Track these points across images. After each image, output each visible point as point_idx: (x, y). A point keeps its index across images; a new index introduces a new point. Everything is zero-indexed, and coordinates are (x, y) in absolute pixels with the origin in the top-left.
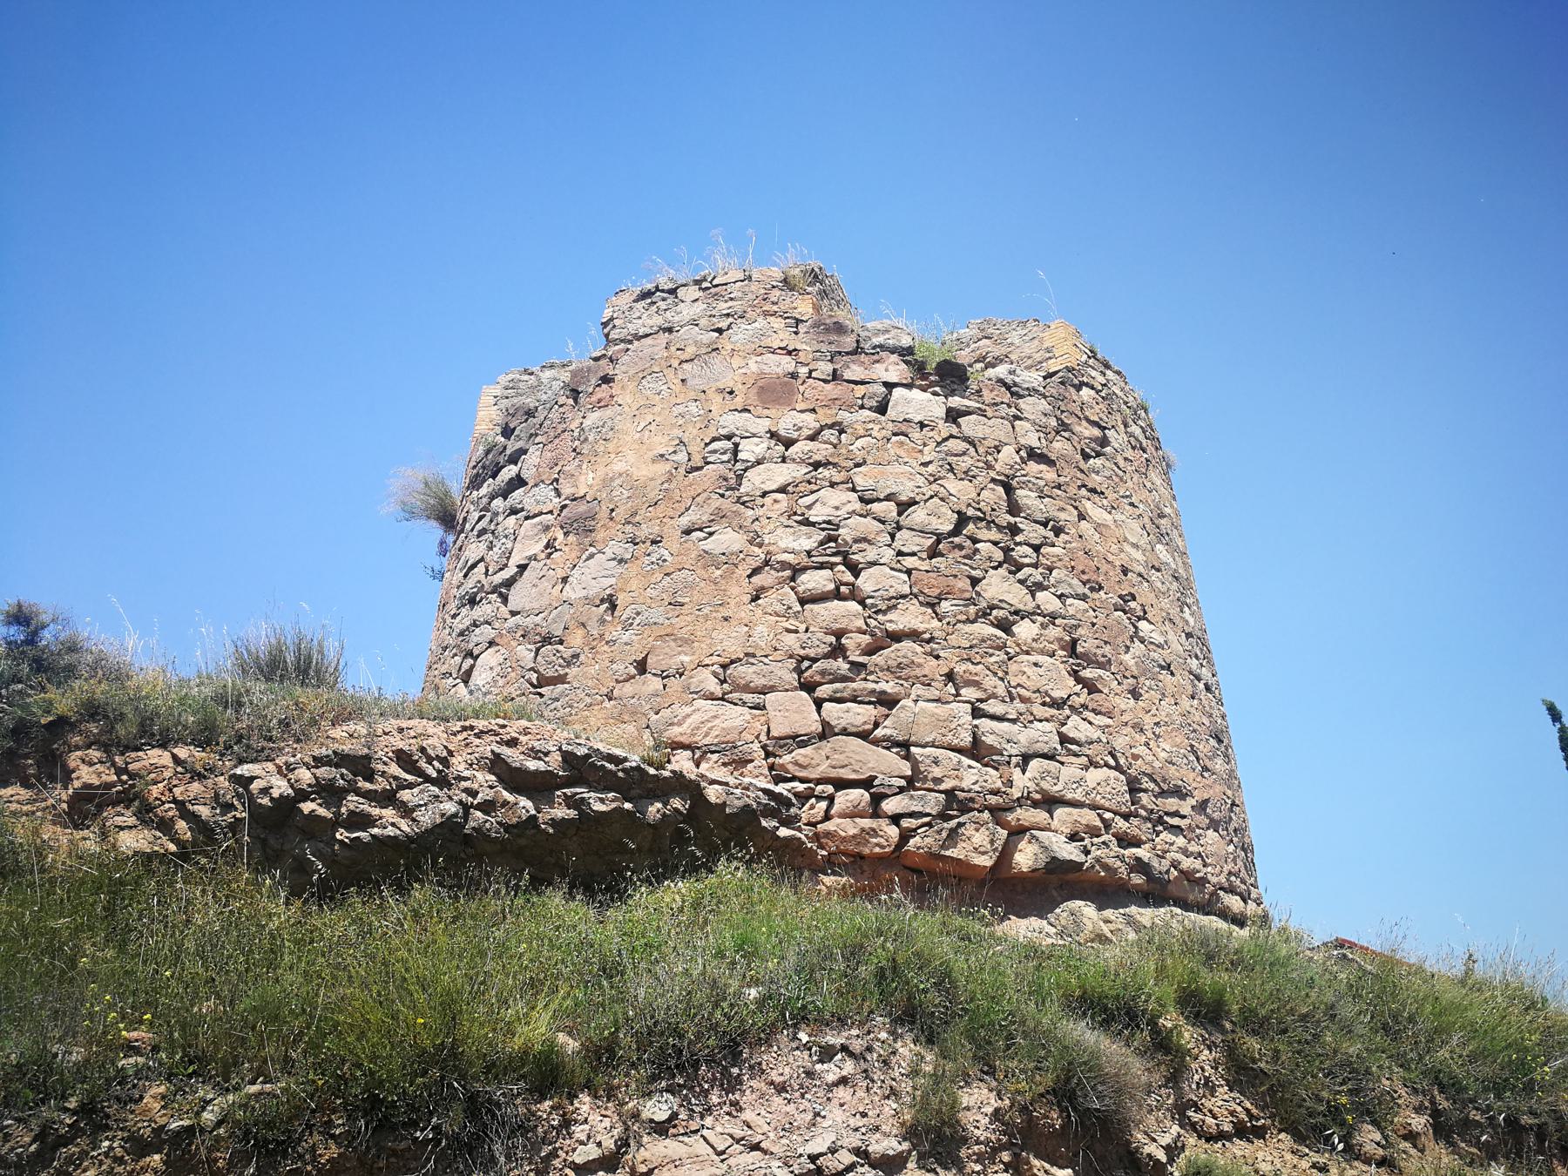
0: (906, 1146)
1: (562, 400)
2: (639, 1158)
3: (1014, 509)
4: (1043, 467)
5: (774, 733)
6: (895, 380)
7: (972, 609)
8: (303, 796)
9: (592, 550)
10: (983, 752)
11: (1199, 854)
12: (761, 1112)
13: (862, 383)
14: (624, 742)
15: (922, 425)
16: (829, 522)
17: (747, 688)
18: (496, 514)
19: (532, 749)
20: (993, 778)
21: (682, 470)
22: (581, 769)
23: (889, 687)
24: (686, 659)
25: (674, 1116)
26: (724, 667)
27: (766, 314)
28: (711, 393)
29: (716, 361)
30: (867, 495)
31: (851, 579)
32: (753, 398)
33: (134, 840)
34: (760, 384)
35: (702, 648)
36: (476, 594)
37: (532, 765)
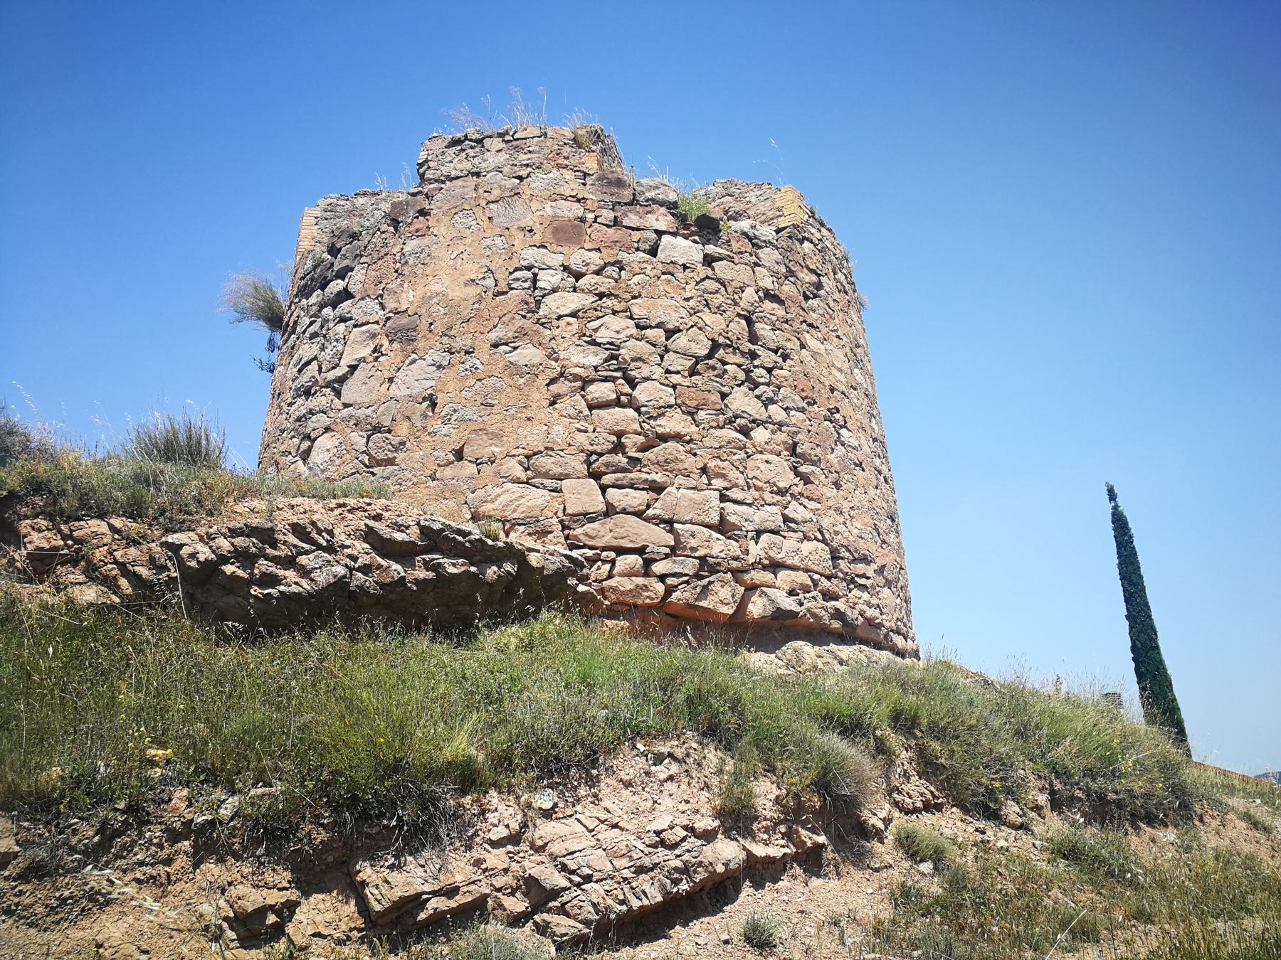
0: (717, 823)
1: (384, 227)
2: (537, 836)
3: (754, 338)
4: (775, 305)
5: (569, 511)
6: (664, 228)
7: (721, 418)
8: (224, 560)
9: (414, 356)
10: (727, 528)
12: (614, 800)
13: (638, 229)
14: (445, 514)
15: (685, 267)
16: (611, 344)
17: (547, 475)
18: (326, 321)
19: (396, 523)
20: (734, 548)
21: (490, 294)
22: (435, 540)
23: (658, 477)
24: (497, 450)
25: (555, 805)
26: (528, 457)
27: (559, 166)
28: (513, 230)
29: (518, 204)
30: (642, 322)
31: (629, 391)
32: (549, 237)
33: (89, 594)
34: (555, 224)
35: (510, 442)
36: (311, 387)
37: (399, 536)
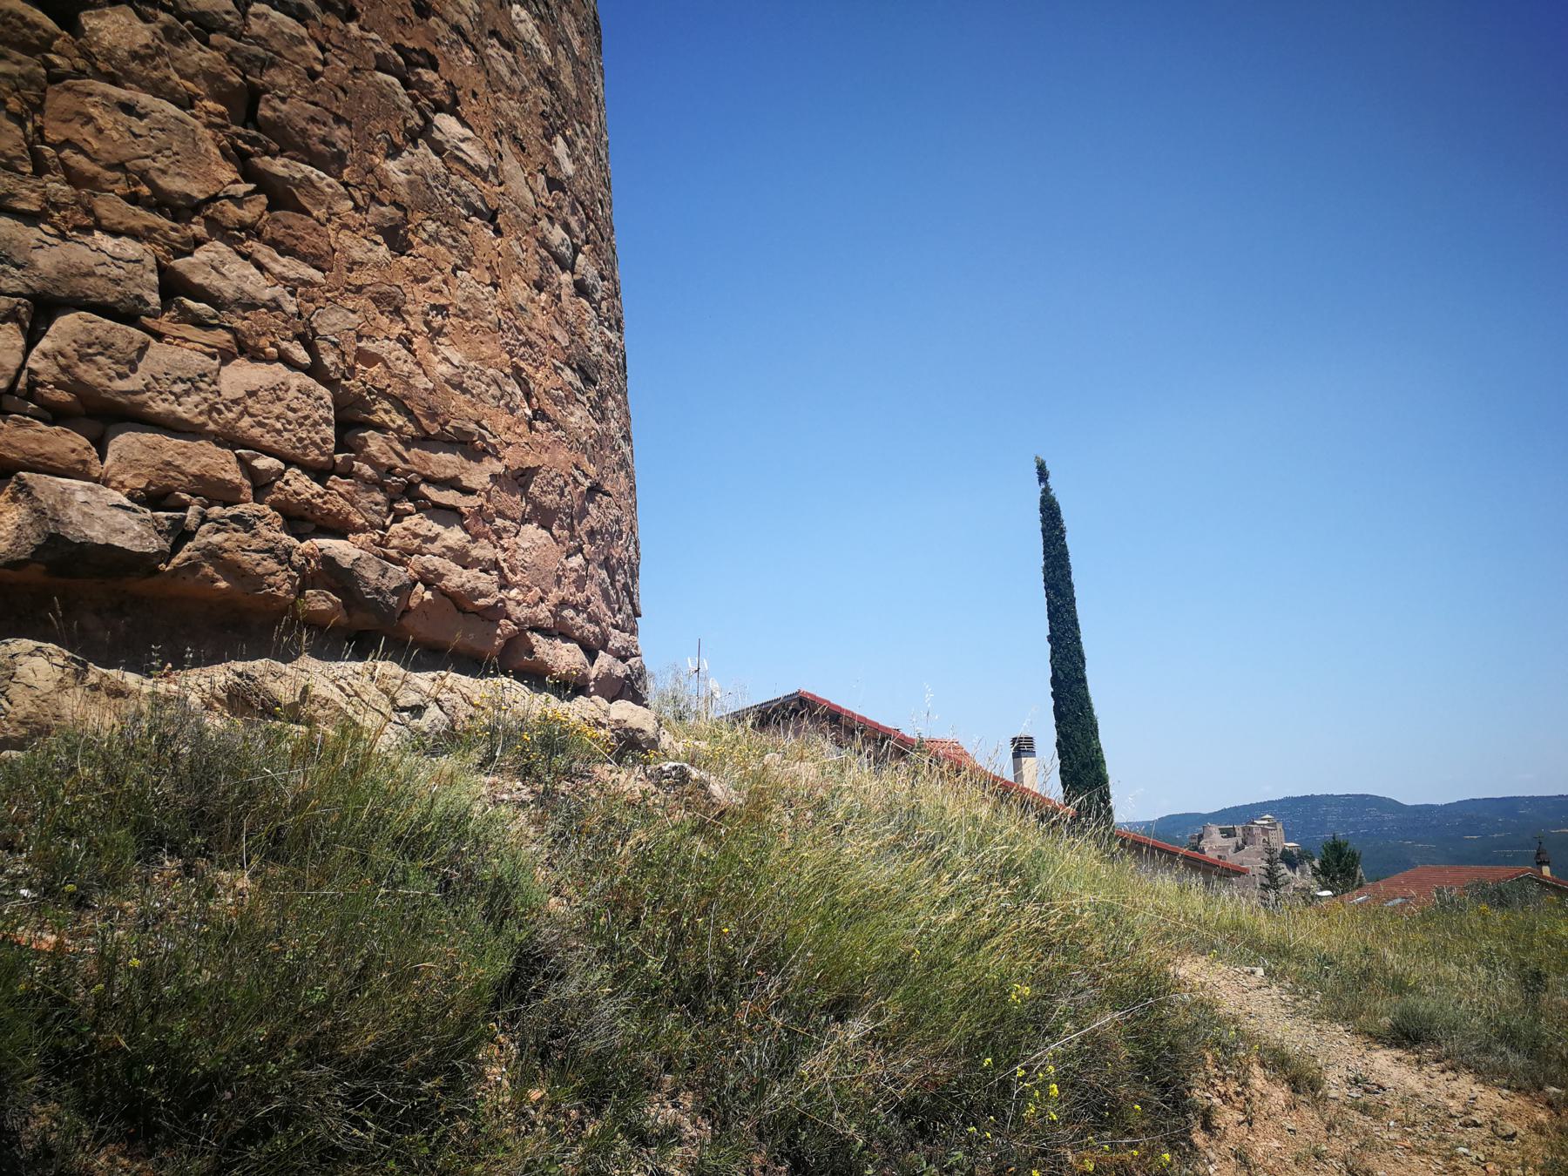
11: (496, 565)
